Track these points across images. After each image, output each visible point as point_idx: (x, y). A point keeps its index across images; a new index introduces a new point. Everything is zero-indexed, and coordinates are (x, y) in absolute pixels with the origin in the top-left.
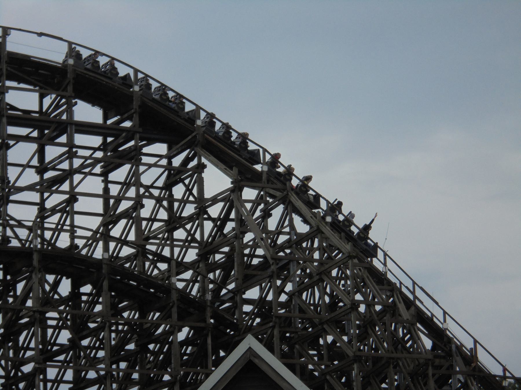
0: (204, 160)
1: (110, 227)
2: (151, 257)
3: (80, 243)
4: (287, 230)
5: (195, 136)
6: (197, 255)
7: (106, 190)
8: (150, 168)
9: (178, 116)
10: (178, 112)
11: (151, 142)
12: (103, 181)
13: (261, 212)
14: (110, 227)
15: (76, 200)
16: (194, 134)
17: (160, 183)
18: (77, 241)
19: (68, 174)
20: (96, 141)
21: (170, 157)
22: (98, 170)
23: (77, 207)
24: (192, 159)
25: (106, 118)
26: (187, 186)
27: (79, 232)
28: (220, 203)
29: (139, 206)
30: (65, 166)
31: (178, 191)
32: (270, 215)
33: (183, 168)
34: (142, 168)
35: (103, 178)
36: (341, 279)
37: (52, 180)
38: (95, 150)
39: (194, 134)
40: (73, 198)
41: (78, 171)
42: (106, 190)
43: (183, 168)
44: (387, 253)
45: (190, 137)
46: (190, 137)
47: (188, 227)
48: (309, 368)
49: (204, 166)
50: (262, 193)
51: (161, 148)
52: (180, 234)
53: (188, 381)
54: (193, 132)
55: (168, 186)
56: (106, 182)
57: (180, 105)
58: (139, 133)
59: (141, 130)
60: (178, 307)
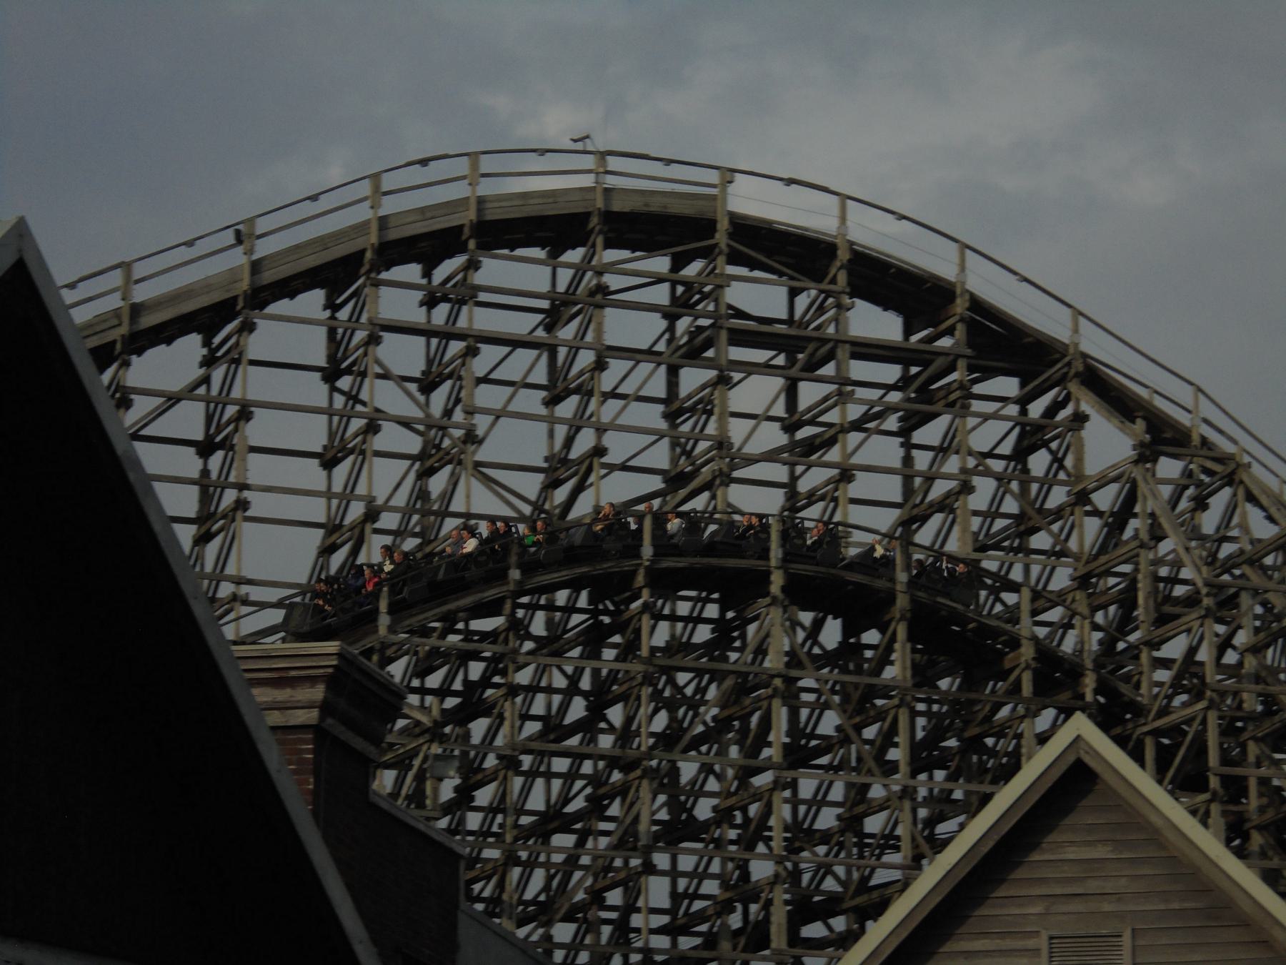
0: (1085, 407)
7: (908, 460)
8: (986, 420)
12: (902, 445)
17: (1006, 448)
20: (891, 373)
22: (892, 423)
25: (908, 332)
31: (1039, 462)
35: (901, 440)
38: (889, 388)
42: (908, 460)
51: (1008, 386)
55: (1021, 454)
56: (908, 446)
59: (969, 352)
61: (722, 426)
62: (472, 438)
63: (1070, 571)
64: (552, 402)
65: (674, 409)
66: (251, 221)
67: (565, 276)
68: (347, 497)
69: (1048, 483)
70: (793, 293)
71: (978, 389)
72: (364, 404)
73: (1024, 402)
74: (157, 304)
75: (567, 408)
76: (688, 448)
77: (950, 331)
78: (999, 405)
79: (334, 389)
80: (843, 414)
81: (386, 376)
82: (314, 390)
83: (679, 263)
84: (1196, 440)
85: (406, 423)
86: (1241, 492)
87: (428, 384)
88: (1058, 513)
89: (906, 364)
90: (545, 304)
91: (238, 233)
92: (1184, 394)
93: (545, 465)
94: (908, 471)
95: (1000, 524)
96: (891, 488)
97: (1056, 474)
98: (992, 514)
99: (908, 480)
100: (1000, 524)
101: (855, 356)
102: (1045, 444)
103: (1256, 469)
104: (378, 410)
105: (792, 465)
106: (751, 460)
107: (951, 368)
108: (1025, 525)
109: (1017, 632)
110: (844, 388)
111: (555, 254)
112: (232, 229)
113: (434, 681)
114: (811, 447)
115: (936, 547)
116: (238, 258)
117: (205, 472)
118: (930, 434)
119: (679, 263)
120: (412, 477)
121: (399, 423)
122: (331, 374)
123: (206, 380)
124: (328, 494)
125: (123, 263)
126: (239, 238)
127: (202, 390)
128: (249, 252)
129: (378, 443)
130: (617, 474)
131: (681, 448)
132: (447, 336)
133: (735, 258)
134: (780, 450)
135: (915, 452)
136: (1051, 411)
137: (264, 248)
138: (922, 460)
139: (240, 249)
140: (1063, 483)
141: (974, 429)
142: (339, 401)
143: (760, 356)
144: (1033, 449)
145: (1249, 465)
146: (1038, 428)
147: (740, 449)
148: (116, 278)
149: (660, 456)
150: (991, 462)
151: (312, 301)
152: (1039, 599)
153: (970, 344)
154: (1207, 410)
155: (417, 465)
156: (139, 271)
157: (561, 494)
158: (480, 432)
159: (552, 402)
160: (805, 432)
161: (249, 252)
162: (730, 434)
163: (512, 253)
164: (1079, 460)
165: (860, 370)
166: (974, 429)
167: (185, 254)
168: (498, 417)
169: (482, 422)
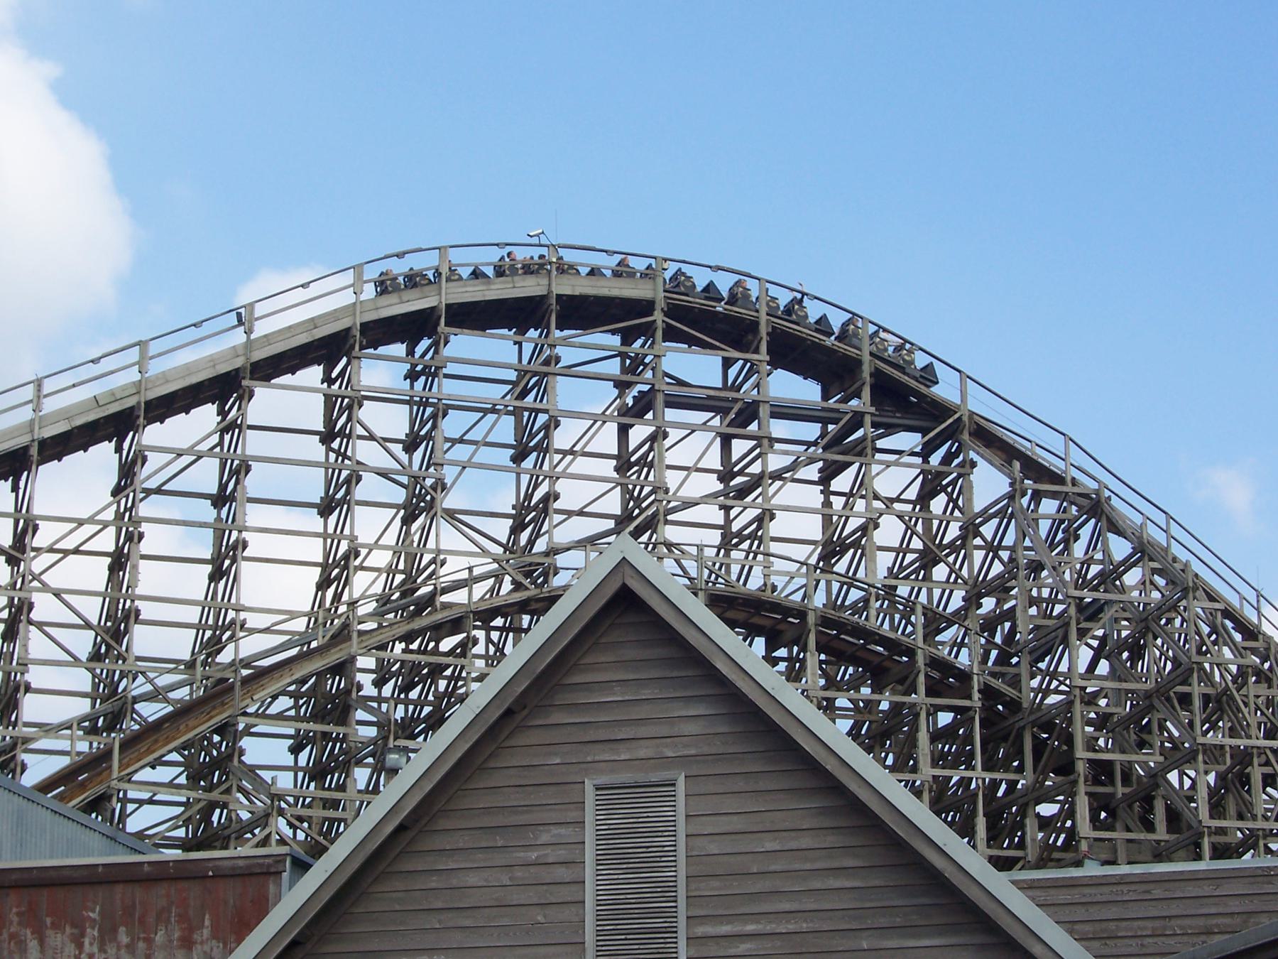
0: (972, 455)
1: (833, 561)
2: (901, 607)
3: (779, 581)
4: (1099, 556)
5: (959, 419)
6: (964, 599)
7: (827, 504)
8: (888, 466)
9: (904, 373)
10: (904, 368)
11: (890, 429)
12: (822, 492)
13: (1063, 533)
14: (833, 561)
15: (772, 517)
16: (956, 416)
17: (912, 494)
18: (774, 579)
19: (757, 481)
20: (811, 431)
21: (925, 453)
22: (812, 472)
23: (775, 528)
24: (956, 455)
25: (826, 397)
26: (950, 495)
27: (778, 564)
28: (994, 519)
29: (1039, 568)
30: (756, 468)
31: (938, 504)
32: (1077, 538)
33: (944, 469)
34: (875, 468)
35: (822, 488)
36: (1048, 601)
37: (739, 487)
38: (809, 444)
39: (956, 416)
40: (766, 516)
41: (777, 476)
42: (827, 504)
43: (944, 469)
44: (1262, 593)
45: (950, 421)
46: (950, 421)
47: (951, 559)
48: (1169, 776)
49: (973, 464)
50: (1065, 504)
51: (909, 440)
52: (940, 572)
53: (80, 778)
54: (956, 413)
55: (924, 498)
56: (827, 493)
57: (771, 303)
58: (872, 414)
59: (873, 410)
60: (927, 676)
61: (660, 477)
62: (441, 486)
63: (964, 593)
64: (518, 458)
65: (623, 465)
66: (250, 306)
67: (528, 348)
68: (336, 537)
69: (945, 521)
70: (727, 363)
71: (881, 444)
72: (349, 459)
73: (925, 453)
74: (65, 414)
75: (528, 463)
76: (636, 494)
77: (858, 395)
78: (897, 456)
79: (329, 449)
80: (764, 464)
81: (372, 437)
82: (314, 449)
83: (627, 341)
84: (1069, 479)
85: (384, 474)
86: (1104, 522)
87: (410, 446)
88: (953, 547)
89: (825, 422)
90: (512, 376)
91: (239, 315)
92: (1056, 443)
93: (514, 512)
94: (827, 511)
95: (910, 557)
96: (812, 528)
97: (952, 513)
98: (902, 550)
99: (827, 520)
100: (910, 557)
101: (775, 415)
102: (944, 489)
103: (1115, 502)
104: (358, 463)
105: (727, 509)
106: (688, 504)
107: (859, 425)
108: (928, 559)
109: (912, 642)
110: (765, 442)
111: (522, 331)
112: (235, 312)
113: (414, 694)
114: (742, 493)
115: (850, 574)
116: (239, 337)
117: (219, 519)
118: (842, 482)
119: (627, 341)
120: (398, 522)
121: (378, 474)
122: (327, 437)
123: (221, 443)
124: (324, 535)
125: (141, 341)
126: (240, 322)
127: (218, 449)
128: (248, 332)
129: (360, 492)
130: (575, 518)
131: (628, 495)
132: (424, 403)
133: (671, 335)
134: (715, 495)
135: (832, 498)
136: (947, 460)
137: (261, 329)
138: (838, 502)
139: (242, 329)
140: (957, 520)
141: (878, 474)
142: (332, 456)
143: (698, 417)
144: (933, 494)
145: (1109, 498)
146: (940, 475)
147: (675, 493)
148: (134, 355)
149: (613, 504)
150: (897, 506)
151: (312, 375)
152: (935, 622)
153: (873, 402)
154: (1077, 456)
155: (402, 512)
156: (48, 387)
157: (524, 537)
158: (448, 481)
159: (518, 458)
160: (739, 480)
161: (248, 332)
162: (667, 480)
163: (1233, 631)
164: (969, 500)
165: (779, 428)
166: (878, 474)
167: (193, 333)
168: (464, 468)
169: (449, 473)
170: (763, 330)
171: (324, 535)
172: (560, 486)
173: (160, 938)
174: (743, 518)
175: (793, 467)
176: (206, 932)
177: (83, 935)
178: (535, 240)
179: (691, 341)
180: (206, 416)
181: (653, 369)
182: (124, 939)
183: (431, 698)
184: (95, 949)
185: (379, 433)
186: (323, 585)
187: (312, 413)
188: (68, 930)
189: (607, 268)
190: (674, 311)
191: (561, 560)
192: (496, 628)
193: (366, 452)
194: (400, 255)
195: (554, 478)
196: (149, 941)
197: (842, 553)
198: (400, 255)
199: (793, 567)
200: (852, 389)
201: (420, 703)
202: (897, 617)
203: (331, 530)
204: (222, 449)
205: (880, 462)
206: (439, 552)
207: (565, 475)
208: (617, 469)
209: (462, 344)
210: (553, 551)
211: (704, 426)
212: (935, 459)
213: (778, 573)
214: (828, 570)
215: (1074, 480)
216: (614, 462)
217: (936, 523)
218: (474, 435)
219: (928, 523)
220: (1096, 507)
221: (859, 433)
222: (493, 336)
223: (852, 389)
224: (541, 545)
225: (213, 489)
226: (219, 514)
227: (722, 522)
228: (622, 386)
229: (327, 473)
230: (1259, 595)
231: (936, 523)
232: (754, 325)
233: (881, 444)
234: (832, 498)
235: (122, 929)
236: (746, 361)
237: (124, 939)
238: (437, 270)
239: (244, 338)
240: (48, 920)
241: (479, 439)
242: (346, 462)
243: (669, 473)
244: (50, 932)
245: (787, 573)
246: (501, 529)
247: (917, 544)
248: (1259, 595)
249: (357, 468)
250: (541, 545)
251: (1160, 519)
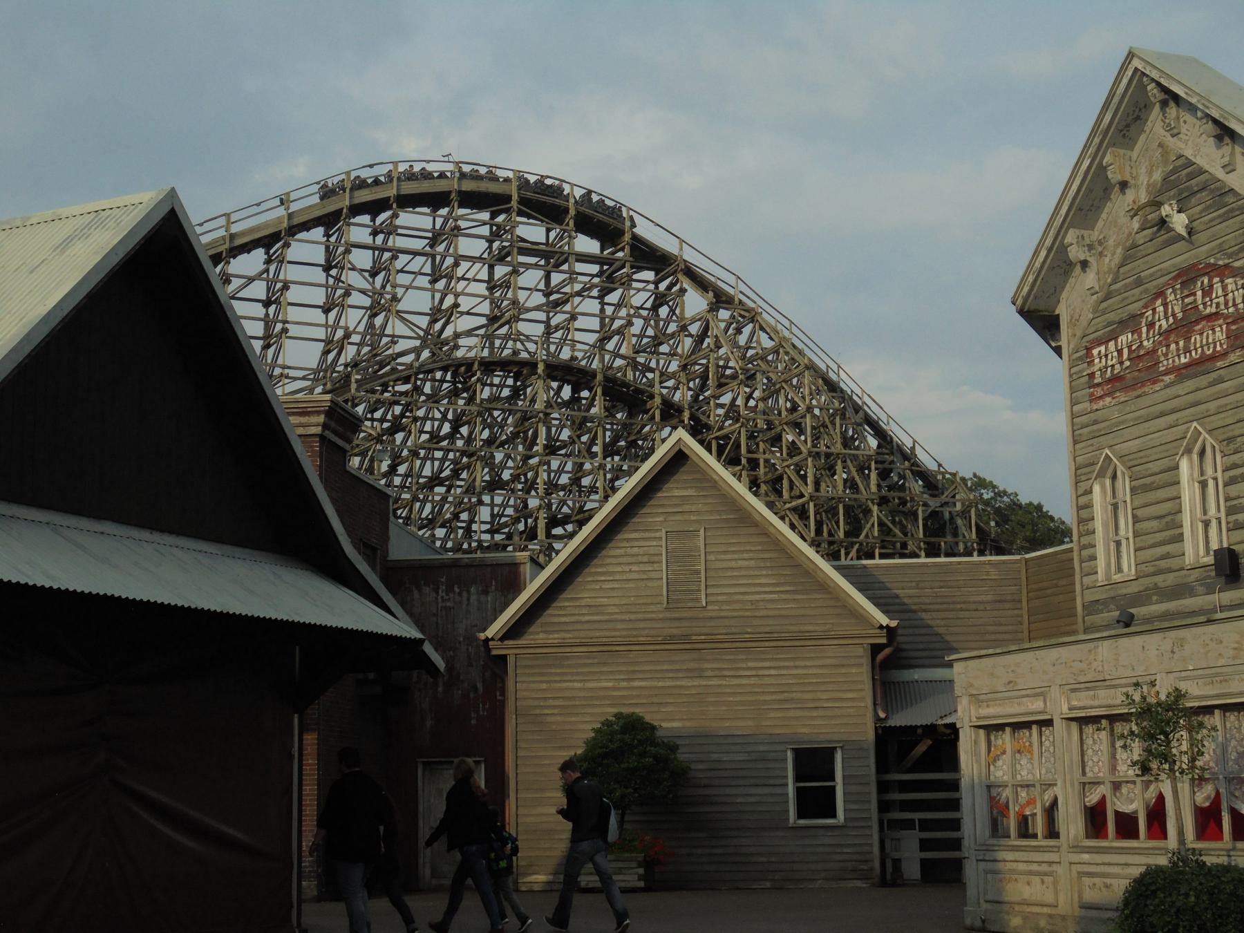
0: (685, 286)
3: (579, 355)
11: (640, 269)
12: (599, 303)
17: (648, 305)
18: (576, 354)
20: (594, 269)
21: (657, 283)
22: (595, 293)
25: (602, 250)
38: (593, 276)
42: (602, 310)
49: (685, 291)
51: (649, 275)
52: (664, 348)
55: (655, 308)
56: (603, 304)
59: (631, 259)
62: (395, 299)
65: (492, 286)
66: (288, 194)
68: (335, 327)
69: (668, 321)
70: (548, 231)
71: (635, 277)
72: (343, 282)
73: (657, 283)
77: (622, 249)
78: (645, 284)
79: (328, 275)
81: (353, 269)
82: (319, 276)
83: (494, 215)
85: (363, 292)
87: (374, 274)
88: (673, 335)
89: (602, 264)
90: (430, 235)
92: (731, 279)
95: (645, 340)
96: (595, 323)
98: (642, 336)
99: (602, 320)
100: (645, 340)
101: (578, 261)
104: (349, 285)
105: (548, 312)
106: (529, 310)
107: (623, 267)
108: (657, 341)
111: (435, 209)
113: (378, 415)
114: (557, 304)
116: (281, 212)
117: (267, 315)
118: (613, 298)
122: (327, 268)
127: (265, 275)
129: (351, 301)
131: (495, 304)
133: (520, 213)
135: (605, 307)
137: (294, 207)
138: (609, 310)
140: (675, 321)
142: (331, 281)
143: (533, 260)
144: (661, 305)
146: (664, 295)
147: (523, 305)
151: (318, 233)
152: (664, 375)
164: (683, 311)
165: (580, 267)
169: (400, 291)
170: (572, 212)
171: (326, 326)
172: (461, 300)
173: (473, 590)
174: (557, 319)
175: (584, 290)
176: (493, 587)
177: (438, 588)
178: (446, 159)
179: (529, 216)
180: (259, 254)
181: (512, 234)
182: (457, 590)
183: (389, 417)
184: (444, 594)
185: (359, 266)
186: (326, 352)
187: (319, 256)
188: (432, 586)
189: (448, 171)
190: (523, 201)
191: (461, 342)
192: (420, 379)
193: (353, 279)
194: (371, 166)
195: (457, 295)
196: (468, 592)
197: (610, 338)
198: (371, 166)
199: (587, 347)
200: (619, 247)
201: (382, 420)
202: (637, 373)
203: (331, 322)
204: (268, 275)
205: (635, 289)
206: (285, 322)
207: (463, 293)
208: (488, 289)
209: (407, 218)
210: (457, 336)
211: (536, 266)
212: (663, 286)
213: (580, 350)
214: (602, 348)
215: (740, 301)
216: (486, 285)
217: (662, 323)
218: (469, 275)
219: (657, 323)
220: (752, 316)
221: (624, 270)
222: (406, 212)
223: (619, 247)
224: (448, 332)
225: (264, 297)
226: (267, 311)
227: (545, 319)
228: (490, 242)
229: (268, 284)
230: (839, 367)
231: (662, 323)
232: (567, 210)
233: (635, 277)
234: (605, 307)
235: (456, 587)
236: (561, 230)
237: (457, 590)
238: (389, 176)
239: (284, 213)
240: (423, 582)
241: (416, 270)
242: (340, 284)
243: (520, 291)
244: (424, 587)
245: (583, 351)
246: (423, 322)
247: (650, 332)
248: (839, 367)
249: (348, 288)
250: (448, 332)
251: (787, 323)
